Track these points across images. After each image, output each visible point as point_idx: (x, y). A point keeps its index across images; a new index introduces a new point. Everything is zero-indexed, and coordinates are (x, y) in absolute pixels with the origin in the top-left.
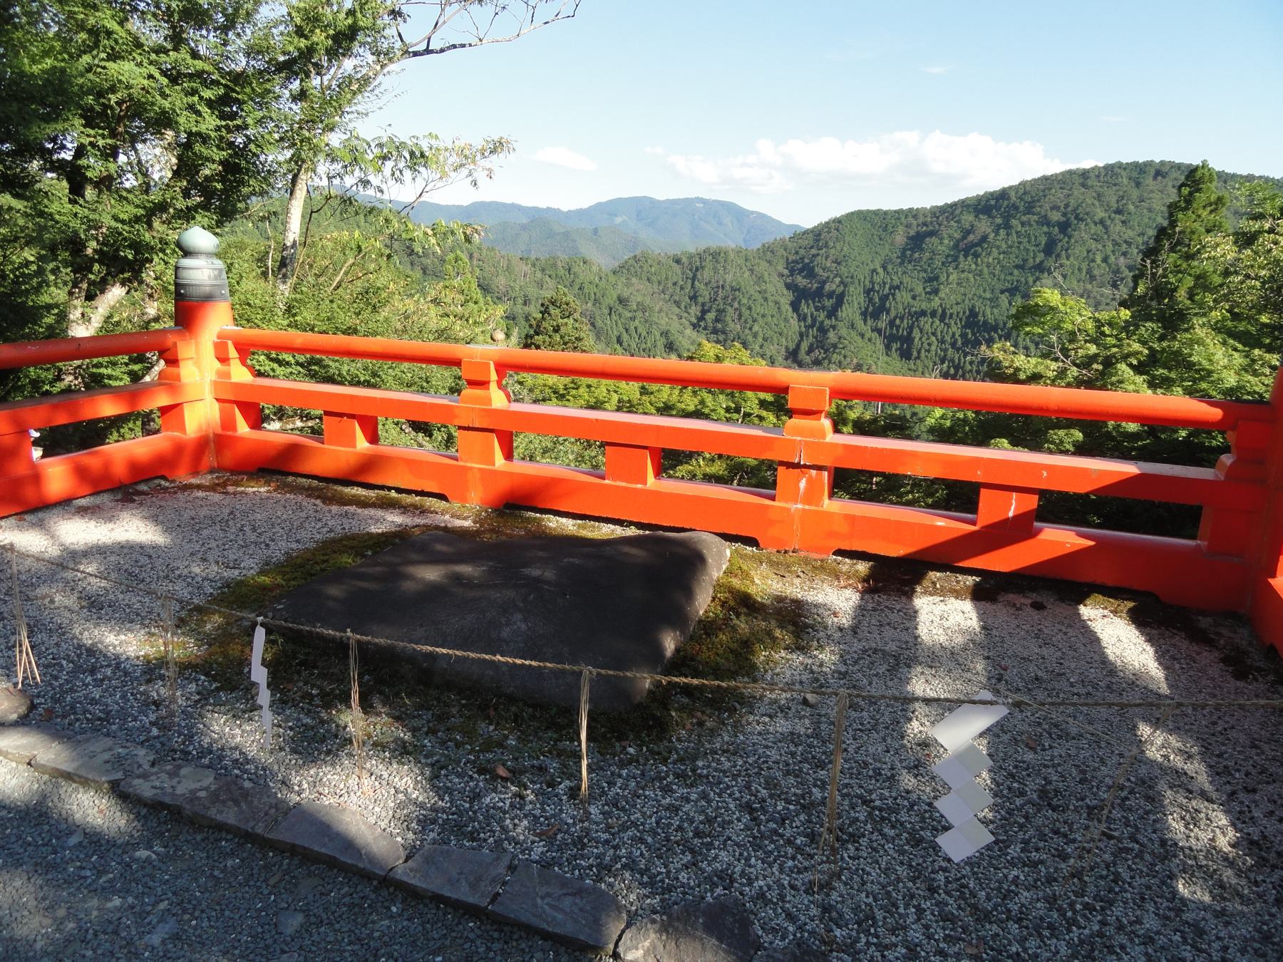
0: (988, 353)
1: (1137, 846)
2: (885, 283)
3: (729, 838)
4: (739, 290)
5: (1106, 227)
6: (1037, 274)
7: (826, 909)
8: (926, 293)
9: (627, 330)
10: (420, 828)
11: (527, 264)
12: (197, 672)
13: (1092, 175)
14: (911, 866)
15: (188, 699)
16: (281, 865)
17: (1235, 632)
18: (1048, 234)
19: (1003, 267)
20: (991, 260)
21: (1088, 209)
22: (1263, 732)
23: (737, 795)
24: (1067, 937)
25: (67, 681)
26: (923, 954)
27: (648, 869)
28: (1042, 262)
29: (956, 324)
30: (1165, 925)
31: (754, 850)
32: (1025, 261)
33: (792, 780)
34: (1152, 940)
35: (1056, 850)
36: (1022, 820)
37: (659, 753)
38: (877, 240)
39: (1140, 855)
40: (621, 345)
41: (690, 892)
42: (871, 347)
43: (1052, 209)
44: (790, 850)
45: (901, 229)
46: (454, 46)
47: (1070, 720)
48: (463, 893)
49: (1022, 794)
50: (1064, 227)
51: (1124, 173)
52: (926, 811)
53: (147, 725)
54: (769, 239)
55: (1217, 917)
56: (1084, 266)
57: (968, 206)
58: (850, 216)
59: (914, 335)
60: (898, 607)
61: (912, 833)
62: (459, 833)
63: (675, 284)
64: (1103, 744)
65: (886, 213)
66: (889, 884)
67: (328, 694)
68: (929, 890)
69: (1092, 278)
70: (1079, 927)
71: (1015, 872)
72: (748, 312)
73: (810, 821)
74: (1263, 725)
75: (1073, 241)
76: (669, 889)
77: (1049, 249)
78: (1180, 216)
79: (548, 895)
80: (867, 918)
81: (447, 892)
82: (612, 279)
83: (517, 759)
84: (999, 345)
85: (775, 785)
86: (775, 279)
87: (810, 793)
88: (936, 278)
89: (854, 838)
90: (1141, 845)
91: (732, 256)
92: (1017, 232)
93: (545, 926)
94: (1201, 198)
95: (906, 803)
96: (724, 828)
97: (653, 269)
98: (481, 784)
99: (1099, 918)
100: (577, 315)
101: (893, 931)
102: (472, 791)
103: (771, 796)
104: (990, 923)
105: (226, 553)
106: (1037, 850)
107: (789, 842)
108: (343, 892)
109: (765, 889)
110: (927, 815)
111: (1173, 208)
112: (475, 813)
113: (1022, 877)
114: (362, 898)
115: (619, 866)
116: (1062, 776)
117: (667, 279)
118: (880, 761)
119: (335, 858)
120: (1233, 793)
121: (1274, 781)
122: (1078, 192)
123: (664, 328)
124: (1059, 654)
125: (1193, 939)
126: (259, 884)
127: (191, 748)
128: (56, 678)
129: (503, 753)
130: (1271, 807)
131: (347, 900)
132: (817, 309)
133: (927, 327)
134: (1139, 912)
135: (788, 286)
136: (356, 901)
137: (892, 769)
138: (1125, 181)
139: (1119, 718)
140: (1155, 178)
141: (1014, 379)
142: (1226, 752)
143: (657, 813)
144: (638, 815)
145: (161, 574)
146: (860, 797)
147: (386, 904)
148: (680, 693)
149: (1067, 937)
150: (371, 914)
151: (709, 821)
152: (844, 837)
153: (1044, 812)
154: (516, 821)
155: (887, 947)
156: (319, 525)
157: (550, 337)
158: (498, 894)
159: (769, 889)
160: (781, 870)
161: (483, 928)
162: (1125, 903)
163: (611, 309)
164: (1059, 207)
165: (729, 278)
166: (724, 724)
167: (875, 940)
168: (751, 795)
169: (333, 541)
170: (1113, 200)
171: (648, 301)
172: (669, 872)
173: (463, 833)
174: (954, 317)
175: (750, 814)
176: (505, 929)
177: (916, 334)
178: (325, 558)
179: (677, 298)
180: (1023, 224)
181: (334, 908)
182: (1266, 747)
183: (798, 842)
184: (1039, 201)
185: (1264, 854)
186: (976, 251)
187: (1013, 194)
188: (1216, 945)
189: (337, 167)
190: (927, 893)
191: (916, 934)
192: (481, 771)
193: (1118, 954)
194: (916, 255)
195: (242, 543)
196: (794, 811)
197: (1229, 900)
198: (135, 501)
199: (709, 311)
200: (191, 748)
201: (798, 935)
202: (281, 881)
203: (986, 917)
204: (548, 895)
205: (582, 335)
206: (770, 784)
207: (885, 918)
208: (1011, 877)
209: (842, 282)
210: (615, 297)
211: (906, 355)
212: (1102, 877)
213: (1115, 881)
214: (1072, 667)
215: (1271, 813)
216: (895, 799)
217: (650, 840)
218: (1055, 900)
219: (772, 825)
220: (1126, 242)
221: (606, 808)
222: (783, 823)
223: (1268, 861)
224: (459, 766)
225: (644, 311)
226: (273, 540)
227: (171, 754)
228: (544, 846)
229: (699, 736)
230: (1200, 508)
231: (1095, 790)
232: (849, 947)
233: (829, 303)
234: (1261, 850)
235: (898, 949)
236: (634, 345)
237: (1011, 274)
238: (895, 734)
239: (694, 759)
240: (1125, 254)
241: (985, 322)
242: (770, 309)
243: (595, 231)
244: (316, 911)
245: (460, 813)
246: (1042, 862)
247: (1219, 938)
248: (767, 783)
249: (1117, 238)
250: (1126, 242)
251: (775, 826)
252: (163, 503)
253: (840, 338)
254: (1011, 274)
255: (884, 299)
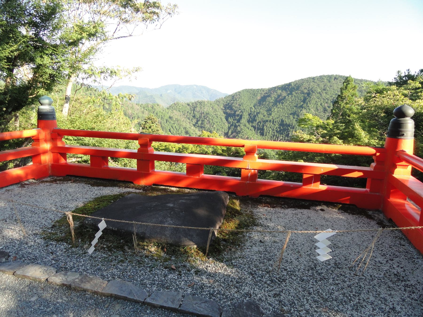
0: (296, 134)
1: (364, 277)
2: (255, 112)
3: (247, 283)
4: (209, 114)
5: (321, 95)
6: (301, 109)
7: (280, 301)
8: (268, 115)
9: (172, 127)
10: (150, 286)
11: (138, 106)
12: (63, 242)
13: (316, 79)
14: (302, 287)
15: (62, 251)
16: (108, 301)
17: (379, 215)
18: (304, 97)
19: (291, 106)
20: (287, 104)
21: (315, 89)
22: (392, 243)
23: (247, 270)
24: (350, 304)
25: (19, 247)
26: (311, 312)
27: (224, 294)
28: (302, 105)
29: (277, 124)
30: (376, 299)
31: (255, 286)
32: (297, 104)
33: (262, 265)
34: (373, 303)
35: (342, 280)
36: (331, 272)
37: (220, 259)
38: (252, 98)
39: (365, 280)
40: (170, 132)
41: (239, 299)
42: (251, 132)
43: (305, 89)
44: (266, 285)
45: (259, 95)
46: (122, 37)
47: (339, 243)
48: (170, 305)
49: (329, 265)
50: (308, 94)
51: (325, 78)
52: (303, 271)
53: (50, 260)
54: (218, 98)
55: (389, 296)
56: (315, 106)
57: (279, 88)
58: (243, 91)
59: (264, 128)
60: (282, 212)
61: (301, 278)
62: (163, 287)
63: (188, 112)
64: (349, 249)
65: (254, 90)
66: (297, 293)
67: (110, 247)
68: (309, 294)
69: (318, 110)
70: (353, 301)
71: (332, 287)
72: (212, 121)
73: (270, 276)
74: (392, 241)
75: (311, 99)
76: (232, 299)
77: (304, 101)
78: (344, 91)
79: (197, 303)
80: (293, 303)
81: (165, 305)
82: (167, 111)
83: (176, 264)
84: (298, 131)
85: (257, 266)
86: (220, 110)
87: (268, 268)
88: (271, 110)
89: (284, 280)
90: (365, 277)
91: (206, 103)
92: (294, 96)
93: (198, 312)
94: (350, 86)
95: (297, 269)
96: (245, 280)
97: (181, 108)
98: (166, 272)
99: (358, 298)
100: (157, 123)
101: (301, 306)
102: (164, 274)
103: (257, 270)
104: (328, 302)
105: (62, 203)
106: (337, 280)
107: (265, 283)
108: (130, 307)
109: (261, 297)
110: (304, 272)
111: (341, 89)
112: (167, 281)
113: (334, 288)
114: (137, 309)
115: (215, 293)
116: (340, 259)
117: (185, 110)
118: (287, 258)
119: (126, 297)
120: (387, 261)
121: (398, 257)
122: (312, 84)
123: (185, 126)
124: (332, 224)
125: (384, 302)
126: (102, 307)
127: (67, 266)
128: (14, 246)
129: (171, 262)
130: (398, 264)
131: (132, 310)
132: (234, 120)
133: (268, 125)
134: (368, 296)
135: (224, 113)
136: (135, 310)
137: (291, 260)
138: (326, 81)
139: (352, 241)
140: (334, 80)
141: (302, 141)
142: (383, 250)
143: (224, 277)
144: (218, 278)
145: (42, 211)
146: (283, 268)
147: (145, 310)
148: (223, 241)
149: (350, 304)
150: (140, 314)
151: (240, 278)
152: (281, 280)
153: (337, 269)
154: (180, 282)
155: (300, 311)
156: (92, 193)
157: (148, 130)
158: (181, 304)
159: (262, 297)
160: (265, 291)
161: (178, 315)
162: (364, 293)
163: (167, 120)
164: (307, 88)
165: (205, 110)
166: (237, 249)
167: (296, 309)
168: (251, 270)
169: (98, 198)
170: (323, 86)
171: (179, 118)
172: (231, 294)
173: (164, 287)
174: (277, 122)
175: (252, 275)
176: (185, 315)
177: (265, 128)
178: (98, 203)
179: (188, 117)
180: (296, 93)
181: (128, 313)
182: (393, 248)
183: (268, 282)
184: (301, 86)
185: (398, 277)
186: (282, 102)
187: (293, 84)
188: (391, 303)
189: (87, 76)
190: (308, 295)
191: (307, 307)
192: (166, 268)
193: (364, 308)
194: (264, 103)
195: (67, 200)
196: (265, 273)
197: (392, 291)
198: (25, 187)
199: (199, 121)
200: (67, 266)
201: (274, 310)
202: (109, 306)
203: (326, 300)
204: (197, 303)
205: (159, 129)
206: (256, 266)
207: (298, 303)
208: (331, 288)
209: (241, 111)
210: (168, 116)
211: (262, 134)
212: (356, 287)
213: (360, 288)
214: (336, 227)
215: (398, 266)
216: (294, 268)
217: (223, 285)
218: (345, 294)
219: (259, 278)
220: (327, 99)
221: (207, 276)
222: (262, 277)
223: (400, 279)
224: (158, 267)
225: (178, 121)
226: (78, 198)
227: (61, 268)
228: (191, 289)
229: (231, 253)
230: (366, 179)
231: (349, 262)
232: (289, 312)
233: (237, 118)
234: (398, 276)
235: (303, 311)
236: (175, 132)
237: (293, 109)
238: (289, 249)
239: (231, 260)
240: (327, 103)
241: (286, 124)
242: (219, 120)
243: (161, 95)
244: (123, 314)
245: (162, 281)
246: (339, 284)
247: (391, 301)
248: (255, 266)
249: (324, 98)
250: (327, 99)
251: (260, 278)
252: (36, 187)
253: (241, 129)
254: (293, 109)
255: (255, 116)
